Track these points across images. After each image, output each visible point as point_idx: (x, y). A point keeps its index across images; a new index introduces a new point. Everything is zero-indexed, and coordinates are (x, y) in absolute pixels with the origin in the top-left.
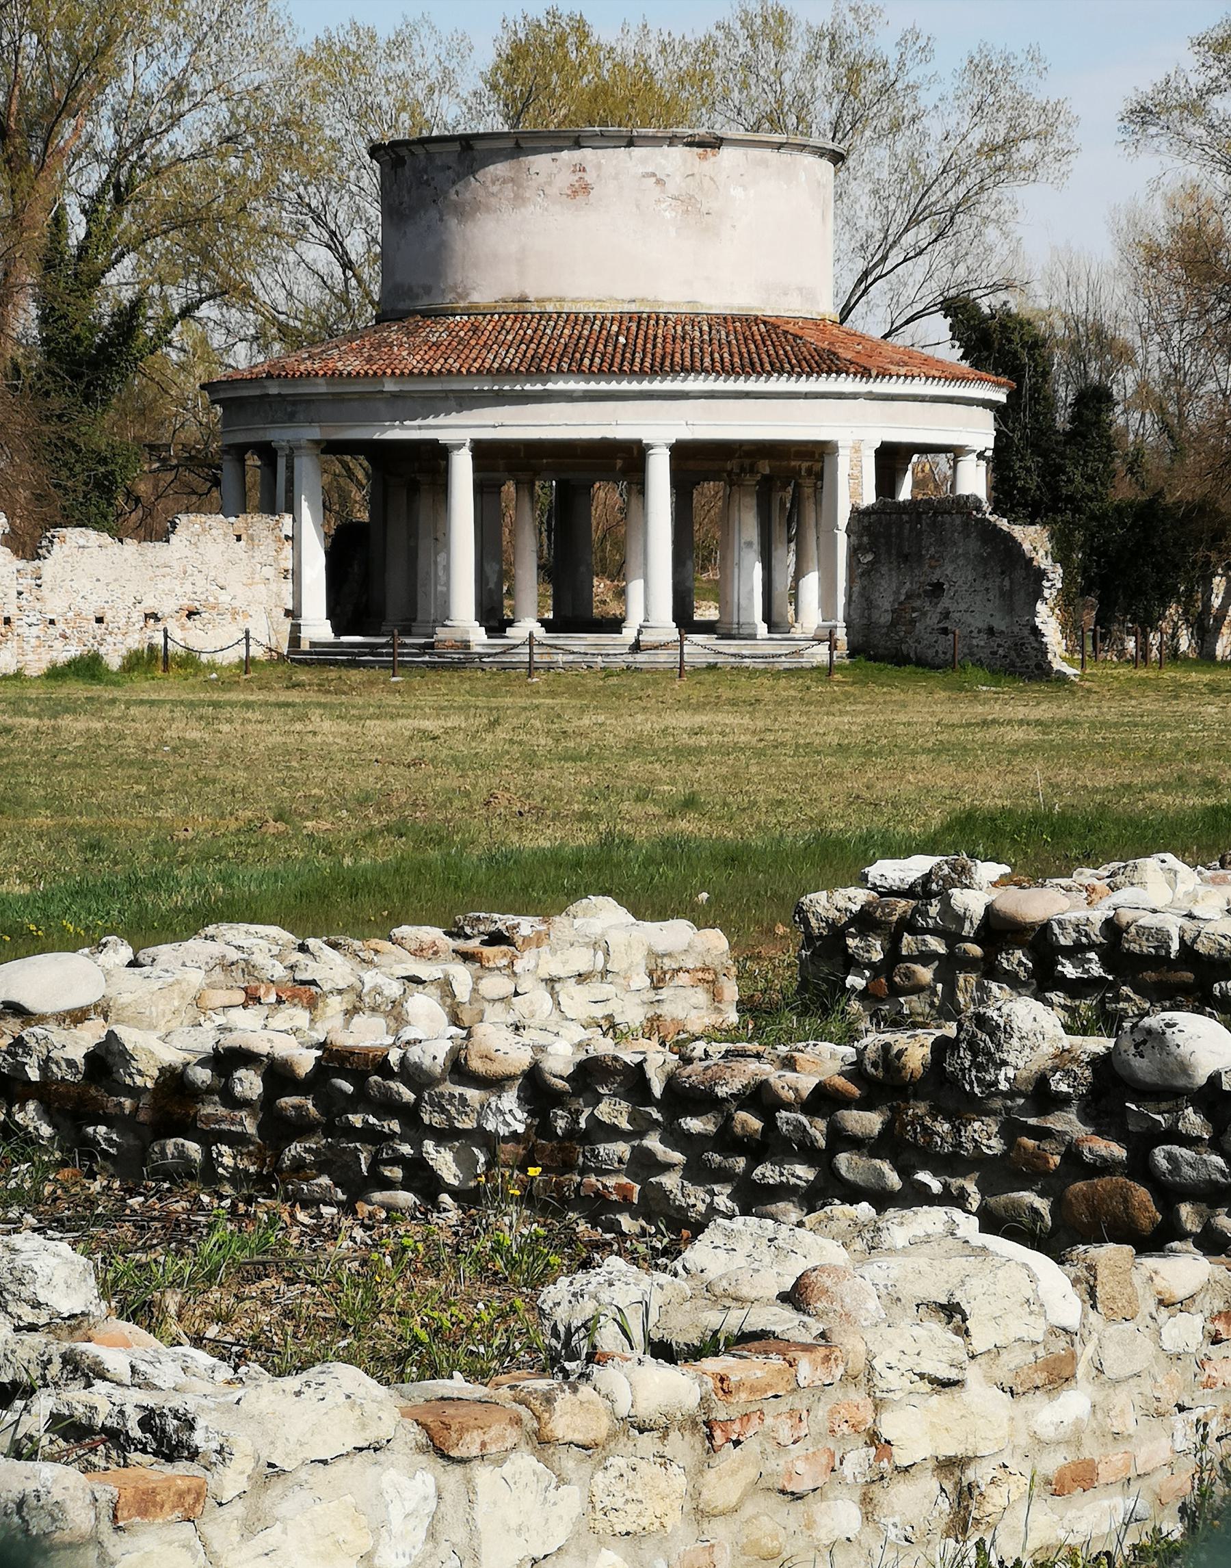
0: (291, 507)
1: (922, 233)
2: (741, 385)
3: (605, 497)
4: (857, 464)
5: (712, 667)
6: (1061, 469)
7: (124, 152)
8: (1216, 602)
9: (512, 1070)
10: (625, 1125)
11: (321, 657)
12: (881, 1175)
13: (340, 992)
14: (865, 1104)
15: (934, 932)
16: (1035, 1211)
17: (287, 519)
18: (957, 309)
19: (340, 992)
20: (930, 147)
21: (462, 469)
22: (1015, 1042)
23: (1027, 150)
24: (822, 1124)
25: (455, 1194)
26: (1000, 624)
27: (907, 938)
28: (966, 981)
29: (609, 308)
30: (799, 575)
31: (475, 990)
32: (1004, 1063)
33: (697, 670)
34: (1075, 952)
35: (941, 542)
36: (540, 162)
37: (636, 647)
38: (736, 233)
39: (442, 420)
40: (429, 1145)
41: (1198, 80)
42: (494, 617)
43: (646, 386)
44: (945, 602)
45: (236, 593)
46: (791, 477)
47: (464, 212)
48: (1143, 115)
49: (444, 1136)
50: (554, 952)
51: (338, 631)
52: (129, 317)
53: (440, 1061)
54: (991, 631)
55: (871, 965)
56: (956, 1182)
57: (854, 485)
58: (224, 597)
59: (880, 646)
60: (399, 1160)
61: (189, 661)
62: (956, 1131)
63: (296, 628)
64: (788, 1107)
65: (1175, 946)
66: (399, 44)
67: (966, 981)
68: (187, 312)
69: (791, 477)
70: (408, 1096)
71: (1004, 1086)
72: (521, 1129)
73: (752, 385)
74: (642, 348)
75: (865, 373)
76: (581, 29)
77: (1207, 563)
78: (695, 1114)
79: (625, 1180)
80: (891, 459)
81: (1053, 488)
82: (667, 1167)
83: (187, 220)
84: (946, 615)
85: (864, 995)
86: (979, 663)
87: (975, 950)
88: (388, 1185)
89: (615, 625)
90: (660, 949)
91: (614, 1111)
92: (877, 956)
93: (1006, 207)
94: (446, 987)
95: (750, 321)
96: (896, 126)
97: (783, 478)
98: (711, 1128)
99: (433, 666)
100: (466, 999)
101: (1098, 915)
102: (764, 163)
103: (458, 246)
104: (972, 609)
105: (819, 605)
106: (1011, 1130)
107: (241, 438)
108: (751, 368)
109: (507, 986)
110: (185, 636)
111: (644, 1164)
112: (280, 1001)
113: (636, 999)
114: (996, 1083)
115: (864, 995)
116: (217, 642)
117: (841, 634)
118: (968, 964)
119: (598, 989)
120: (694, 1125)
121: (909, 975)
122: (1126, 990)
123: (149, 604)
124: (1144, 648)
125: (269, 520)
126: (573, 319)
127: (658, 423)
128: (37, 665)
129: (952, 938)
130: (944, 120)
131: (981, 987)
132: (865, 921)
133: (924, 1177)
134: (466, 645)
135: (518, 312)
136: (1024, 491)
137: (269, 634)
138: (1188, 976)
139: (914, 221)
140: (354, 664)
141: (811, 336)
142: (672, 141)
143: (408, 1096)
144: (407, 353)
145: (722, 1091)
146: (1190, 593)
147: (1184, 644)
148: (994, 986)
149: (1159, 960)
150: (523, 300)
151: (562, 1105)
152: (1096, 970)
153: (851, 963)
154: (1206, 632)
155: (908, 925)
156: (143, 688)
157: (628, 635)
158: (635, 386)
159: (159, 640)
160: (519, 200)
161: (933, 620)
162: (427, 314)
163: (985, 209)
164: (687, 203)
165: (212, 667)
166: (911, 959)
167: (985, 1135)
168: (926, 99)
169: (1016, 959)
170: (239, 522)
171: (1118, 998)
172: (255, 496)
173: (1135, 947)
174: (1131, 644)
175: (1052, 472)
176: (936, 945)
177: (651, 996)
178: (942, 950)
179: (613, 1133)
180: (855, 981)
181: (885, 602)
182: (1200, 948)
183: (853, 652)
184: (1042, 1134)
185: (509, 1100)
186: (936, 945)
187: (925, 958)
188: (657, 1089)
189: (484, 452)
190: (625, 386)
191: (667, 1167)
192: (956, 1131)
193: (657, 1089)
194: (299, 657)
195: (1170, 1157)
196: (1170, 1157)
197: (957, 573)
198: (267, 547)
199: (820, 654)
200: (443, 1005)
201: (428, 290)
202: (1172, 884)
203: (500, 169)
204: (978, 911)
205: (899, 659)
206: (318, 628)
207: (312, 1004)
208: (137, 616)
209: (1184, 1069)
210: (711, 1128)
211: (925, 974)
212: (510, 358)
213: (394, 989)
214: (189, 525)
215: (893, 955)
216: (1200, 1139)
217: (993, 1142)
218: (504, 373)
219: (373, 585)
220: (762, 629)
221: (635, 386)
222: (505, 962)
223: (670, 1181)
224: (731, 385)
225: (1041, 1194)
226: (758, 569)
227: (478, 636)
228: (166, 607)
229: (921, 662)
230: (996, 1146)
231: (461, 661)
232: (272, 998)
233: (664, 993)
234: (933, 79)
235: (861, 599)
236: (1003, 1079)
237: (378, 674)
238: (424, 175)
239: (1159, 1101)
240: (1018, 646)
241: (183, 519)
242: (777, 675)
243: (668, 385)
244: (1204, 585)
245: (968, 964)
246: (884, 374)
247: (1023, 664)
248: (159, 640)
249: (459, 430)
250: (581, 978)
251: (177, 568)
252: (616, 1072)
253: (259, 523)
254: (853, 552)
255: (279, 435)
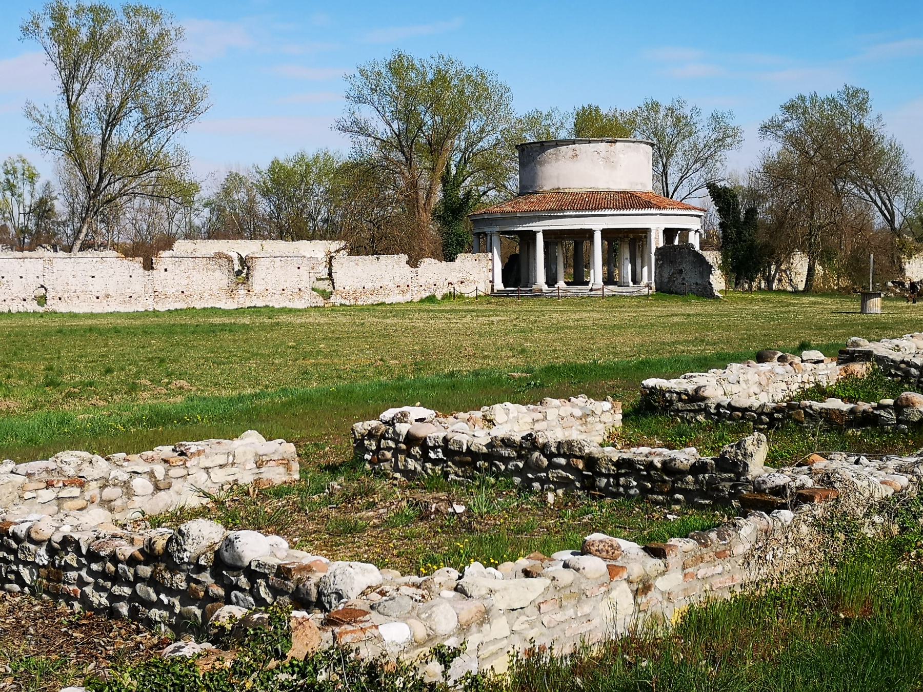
0: (657, 248)
1: (698, 165)
2: (622, 212)
3: (586, 244)
4: (657, 235)
5: (614, 295)
6: (742, 232)
7: (466, 149)
8: (773, 273)
9: (44, 538)
10: (76, 565)
11: (500, 294)
12: (149, 595)
13: (96, 480)
14: (146, 564)
15: (391, 439)
16: (195, 615)
17: (490, 254)
18: (712, 187)
19: (96, 480)
20: (700, 140)
21: (540, 238)
22: (190, 540)
23: (729, 140)
24: (132, 570)
25: (29, 586)
26: (699, 282)
27: (383, 441)
28: (401, 457)
29: (584, 190)
30: (642, 267)
31: (167, 474)
32: (185, 550)
33: (609, 296)
34: (434, 448)
35: (682, 257)
36: (563, 148)
37: (591, 290)
38: (625, 167)
39: (534, 224)
40: (21, 566)
41: (781, 118)
42: (551, 281)
43: (593, 213)
44: (683, 275)
45: (475, 276)
46: (640, 239)
47: (541, 164)
48: (765, 129)
49: (26, 563)
50: (207, 457)
51: (505, 287)
52: (468, 195)
53: (24, 532)
54: (697, 284)
55: (372, 451)
56: (173, 600)
57: (657, 241)
58: (472, 277)
59: (666, 288)
60: (12, 572)
61: (461, 296)
62: (172, 578)
63: (493, 286)
64: (121, 562)
65: (465, 448)
66: (549, 115)
67: (401, 457)
68: (484, 193)
69: (640, 239)
70: (15, 546)
71: (186, 560)
72: (46, 563)
73: (625, 212)
74: (594, 202)
75: (659, 208)
76: (597, 110)
77: (769, 262)
78: (96, 562)
79: (76, 588)
80: (669, 233)
81: (740, 238)
82: (88, 584)
83: (484, 167)
84: (684, 279)
85: (370, 462)
86: (694, 293)
87: (403, 446)
88: (11, 582)
89: (587, 283)
90: (261, 453)
91: (71, 558)
92: (374, 448)
93: (723, 157)
94: (151, 474)
95: (632, 194)
96: (690, 134)
97: (636, 239)
98: (100, 568)
99: (531, 297)
100: (162, 478)
101: (442, 435)
102: (630, 147)
103: (540, 174)
104: (691, 277)
105: (648, 274)
106: (189, 580)
107: (478, 231)
108: (625, 207)
109: (183, 472)
110: (460, 289)
111: (81, 583)
112: (64, 485)
113: (250, 472)
114: (183, 559)
115: (370, 462)
116: (468, 290)
117: (653, 285)
118: (402, 452)
119: (230, 470)
120: (95, 567)
121: (383, 455)
122: (450, 463)
123: (449, 280)
124: (750, 287)
125: (485, 255)
126: (573, 194)
127: (597, 224)
128: (416, 299)
129: (397, 442)
130: (704, 133)
131: (406, 461)
132: (371, 435)
133: (162, 596)
134: (541, 290)
135: (557, 192)
136: (731, 239)
137: (484, 288)
138: (469, 459)
139: (696, 162)
140: (508, 296)
141: (644, 197)
142: (602, 141)
143: (15, 546)
144: (524, 205)
145: (102, 554)
146: (764, 270)
147: (763, 286)
148: (409, 460)
149: (459, 453)
150: (559, 189)
151: (58, 554)
152: (441, 455)
153: (367, 451)
154: (769, 282)
155: (383, 437)
156: (447, 306)
157: (590, 286)
158: (590, 213)
159: (452, 290)
160: (557, 160)
161: (680, 281)
162: (531, 194)
163: (717, 158)
164: (606, 159)
165: (468, 298)
166: (384, 449)
167: (180, 581)
168: (699, 127)
169: (416, 451)
170: (476, 255)
171: (447, 466)
172: (476, 247)
173: (452, 447)
174: (746, 286)
175: (739, 233)
176: (392, 444)
177: (257, 471)
178: (394, 446)
179: (72, 568)
180: (368, 457)
181: (666, 276)
182: (472, 448)
183: (657, 290)
184: (198, 582)
185: (42, 551)
186: (392, 444)
187: (389, 449)
188: (84, 551)
189: (545, 232)
190: (587, 213)
191: (88, 584)
192: (172, 578)
193: (84, 551)
194: (495, 294)
195: (236, 597)
196: (236, 597)
197: (686, 267)
198: (484, 262)
199: (645, 291)
200: (151, 481)
201: (532, 186)
202: (507, 414)
203: (551, 151)
204: (404, 433)
205: (671, 292)
206: (499, 285)
207: (82, 485)
208: (446, 283)
209: (240, 558)
210: (100, 568)
211: (389, 455)
212: (553, 206)
213: (126, 477)
214: (461, 257)
215: (379, 448)
216: (245, 589)
217: (183, 584)
218: (552, 210)
219: (516, 273)
220: (631, 284)
221: (590, 213)
222: (181, 463)
223: (88, 590)
224: (619, 212)
225: (199, 608)
226: (630, 265)
227: (545, 288)
228: (454, 281)
229: (676, 293)
230: (183, 586)
231: (540, 295)
232: (61, 484)
233: (262, 470)
234: (701, 121)
235: (659, 274)
236: (186, 556)
237: (515, 299)
238: (531, 153)
239: (234, 571)
240: (705, 288)
241: (459, 255)
242: (632, 297)
243: (600, 212)
244: (662, 282)
245: (402, 452)
246: (665, 208)
247: (706, 292)
248: (452, 290)
249: (539, 227)
250: (221, 466)
251: (458, 269)
252: (72, 542)
253: (482, 255)
254: (656, 261)
255: (487, 230)
